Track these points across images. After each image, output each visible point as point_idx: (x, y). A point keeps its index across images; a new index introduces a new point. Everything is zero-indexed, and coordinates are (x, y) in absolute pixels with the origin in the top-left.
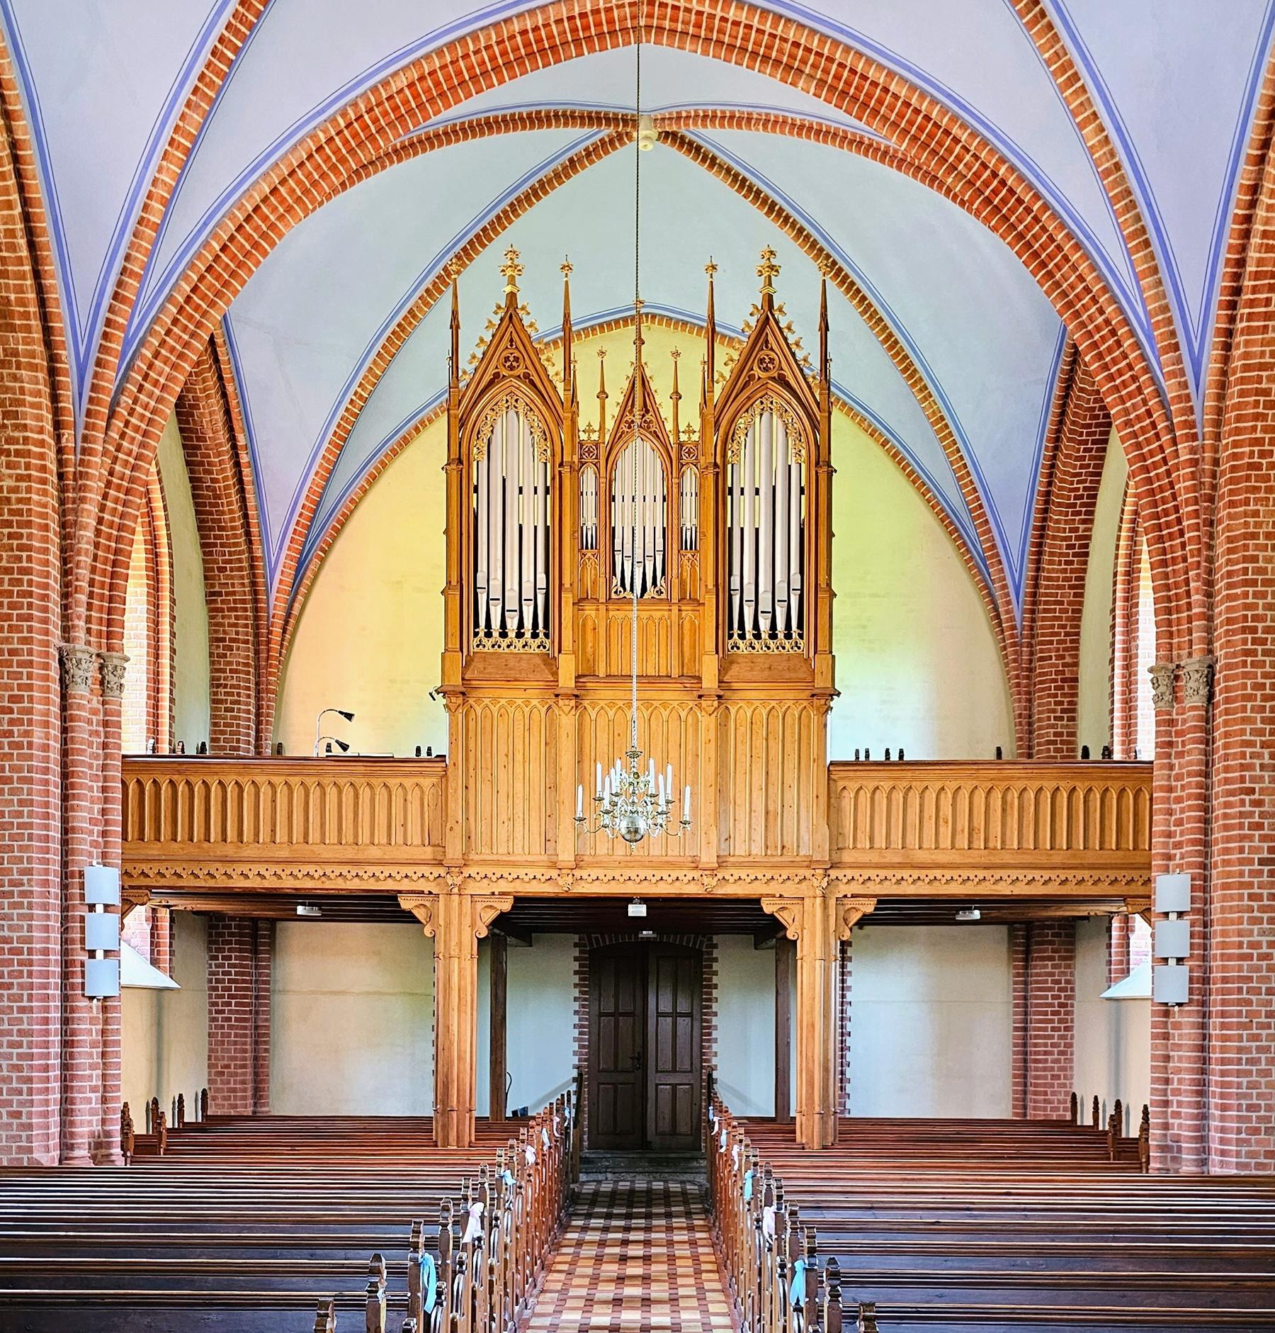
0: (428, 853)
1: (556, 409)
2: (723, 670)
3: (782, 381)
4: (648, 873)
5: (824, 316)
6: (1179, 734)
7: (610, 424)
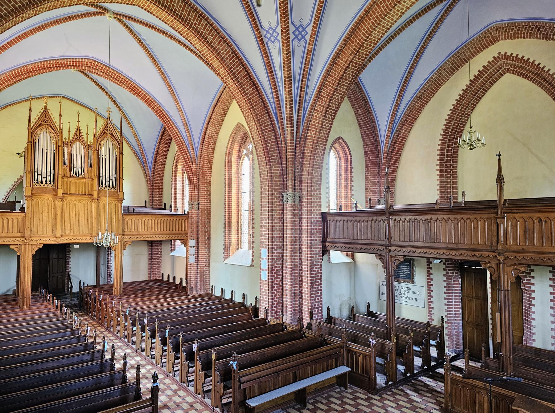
0: (19, 234)
1: (57, 133)
2: (98, 194)
3: (112, 134)
4: (79, 238)
7: (71, 138)
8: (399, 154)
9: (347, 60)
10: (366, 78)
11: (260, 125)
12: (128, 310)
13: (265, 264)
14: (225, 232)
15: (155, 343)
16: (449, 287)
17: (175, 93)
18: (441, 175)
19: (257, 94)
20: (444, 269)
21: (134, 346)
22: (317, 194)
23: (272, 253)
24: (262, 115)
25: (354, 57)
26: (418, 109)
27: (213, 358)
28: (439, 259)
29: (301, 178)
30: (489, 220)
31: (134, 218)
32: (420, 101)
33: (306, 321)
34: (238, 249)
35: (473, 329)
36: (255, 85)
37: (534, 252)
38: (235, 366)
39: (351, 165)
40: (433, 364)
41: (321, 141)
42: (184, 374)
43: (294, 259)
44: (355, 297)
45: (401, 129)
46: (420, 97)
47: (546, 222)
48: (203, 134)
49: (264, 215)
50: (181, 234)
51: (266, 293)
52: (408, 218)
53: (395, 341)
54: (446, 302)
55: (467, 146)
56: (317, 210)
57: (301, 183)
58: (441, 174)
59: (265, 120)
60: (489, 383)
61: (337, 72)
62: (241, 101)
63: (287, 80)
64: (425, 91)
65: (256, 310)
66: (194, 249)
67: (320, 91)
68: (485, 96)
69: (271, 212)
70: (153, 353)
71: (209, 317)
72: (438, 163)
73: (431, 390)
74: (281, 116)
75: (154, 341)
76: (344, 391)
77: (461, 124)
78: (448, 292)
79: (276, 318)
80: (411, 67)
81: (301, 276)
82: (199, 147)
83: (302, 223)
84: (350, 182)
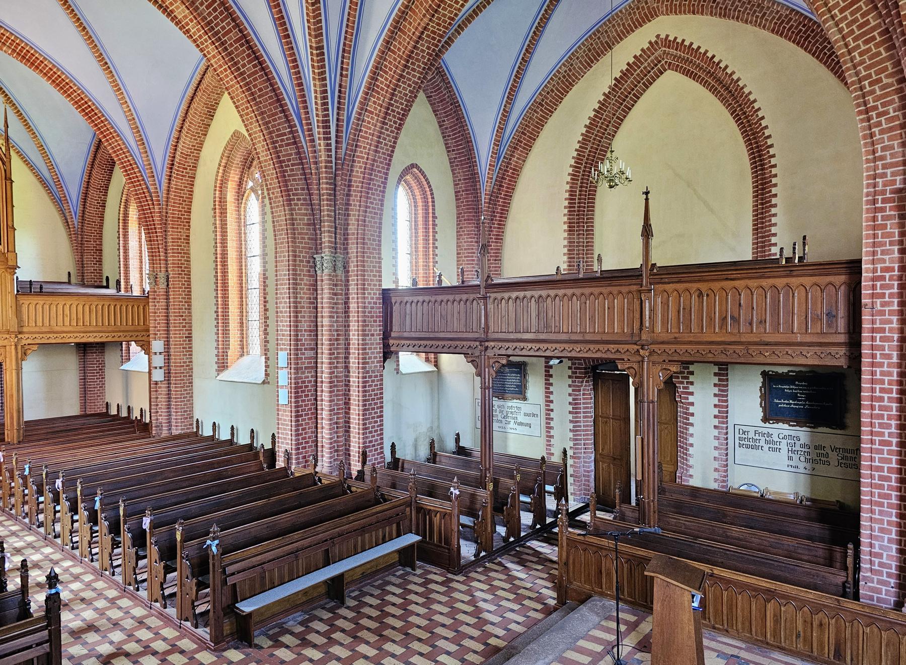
5: (6, 122)
6: (158, 295)
8: (509, 196)
9: (419, 24)
10: (452, 59)
11: (270, 133)
12: (27, 467)
13: (284, 377)
14: (217, 326)
15: (77, 521)
16: (576, 404)
17: (112, 68)
18: (570, 231)
19: (261, 77)
20: (570, 377)
21: (42, 530)
22: (375, 258)
23: (297, 359)
24: (273, 115)
25: (430, 20)
26: (537, 123)
27: (178, 537)
28: (558, 358)
29: (347, 229)
30: (630, 295)
31: (41, 303)
32: (541, 110)
33: (356, 467)
34: (242, 355)
35: (609, 466)
36: (257, 58)
37: (690, 343)
38: (214, 549)
39: (434, 213)
40: (549, 520)
41: (380, 166)
42: (130, 570)
43: (336, 367)
44: (438, 427)
45: (511, 155)
46: (540, 104)
47: (708, 295)
48: (170, 149)
49: (281, 293)
50: (137, 331)
51: (287, 425)
52: (514, 295)
53: (491, 489)
54: (571, 426)
55: (605, 182)
56: (375, 285)
57: (346, 239)
58: (570, 230)
59: (279, 124)
60: (615, 540)
61: (403, 44)
62: (232, 86)
63: (315, 52)
64: (548, 93)
65: (271, 455)
66: (162, 356)
67: (374, 77)
68: (636, 105)
69: (294, 289)
70: (75, 539)
71: (184, 471)
72: (566, 211)
73: (543, 560)
74: (308, 119)
75: (76, 517)
76: (409, 573)
77: (601, 150)
78: (575, 412)
79: (305, 467)
80: (527, 50)
81: (348, 395)
82: (164, 172)
83: (349, 308)
84: (431, 241)
